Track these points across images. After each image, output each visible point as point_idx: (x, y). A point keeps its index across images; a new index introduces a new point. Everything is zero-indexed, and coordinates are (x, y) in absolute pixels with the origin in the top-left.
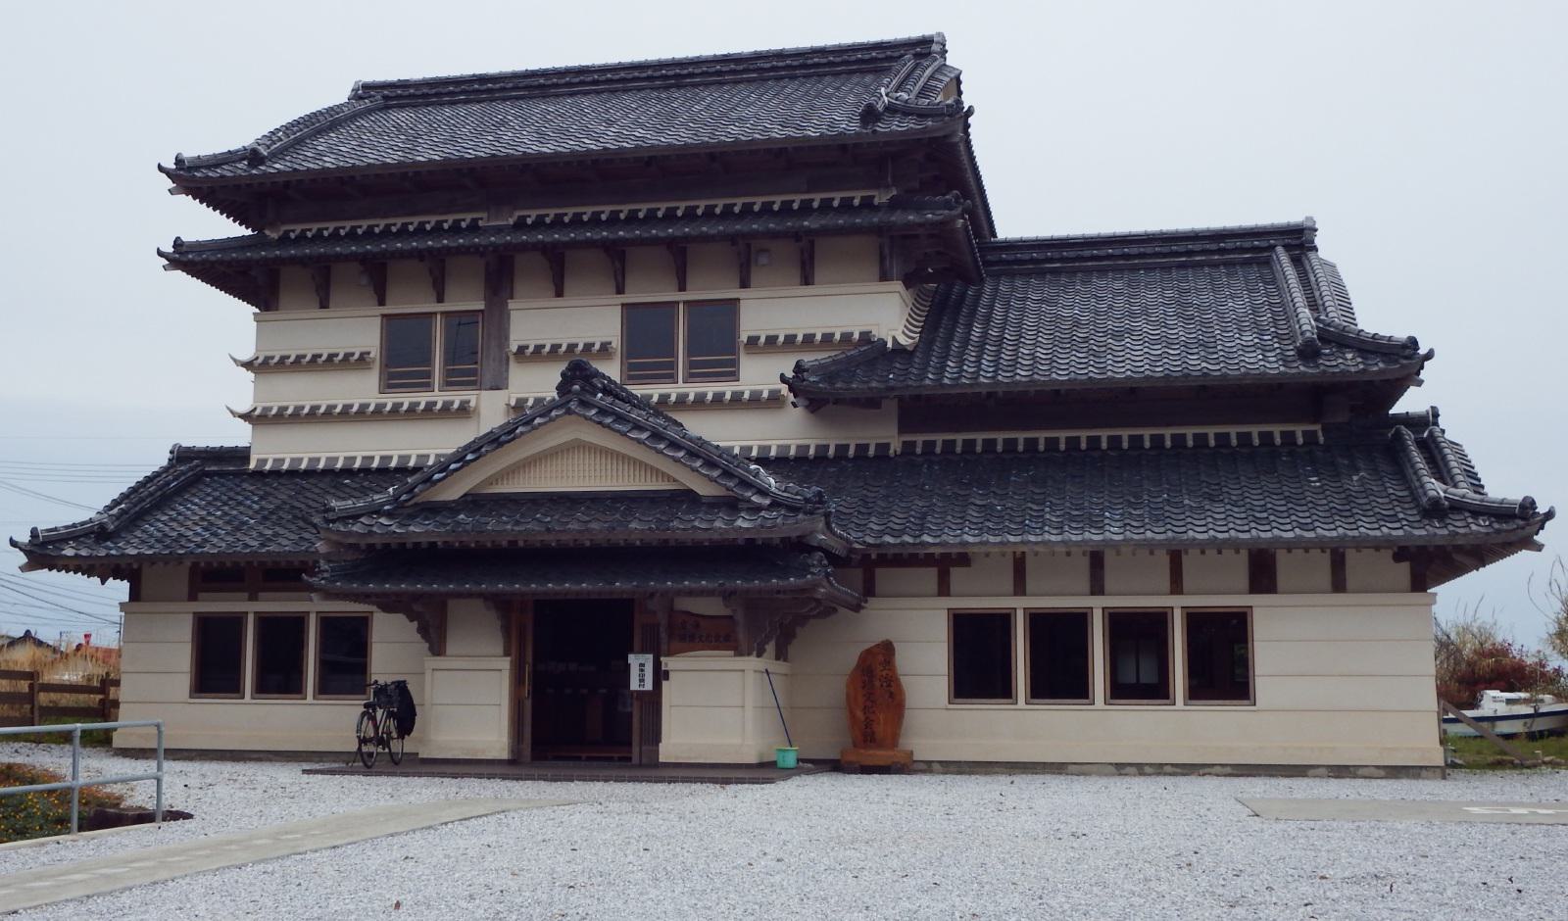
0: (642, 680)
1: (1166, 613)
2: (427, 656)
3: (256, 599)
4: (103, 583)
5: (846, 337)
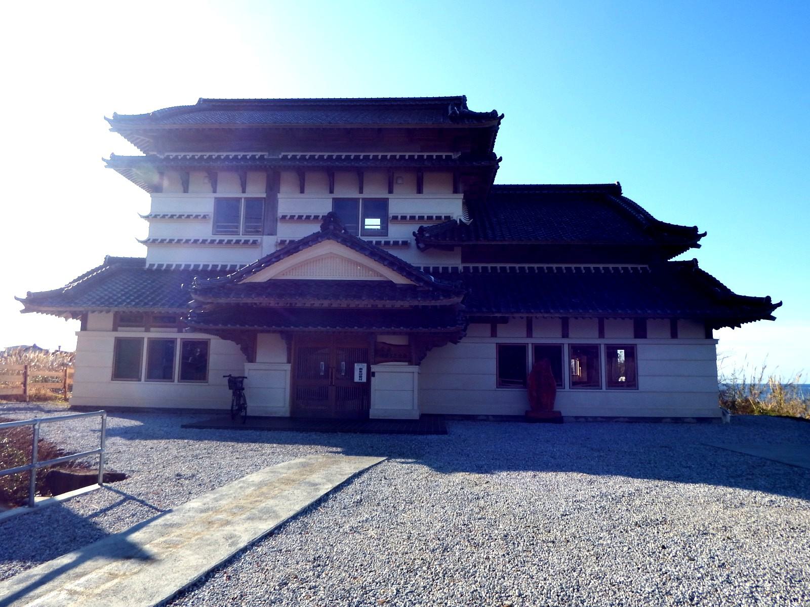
0: (361, 377)
1: (525, 346)
2: (246, 362)
3: (149, 331)
4: (66, 320)
5: (439, 218)
